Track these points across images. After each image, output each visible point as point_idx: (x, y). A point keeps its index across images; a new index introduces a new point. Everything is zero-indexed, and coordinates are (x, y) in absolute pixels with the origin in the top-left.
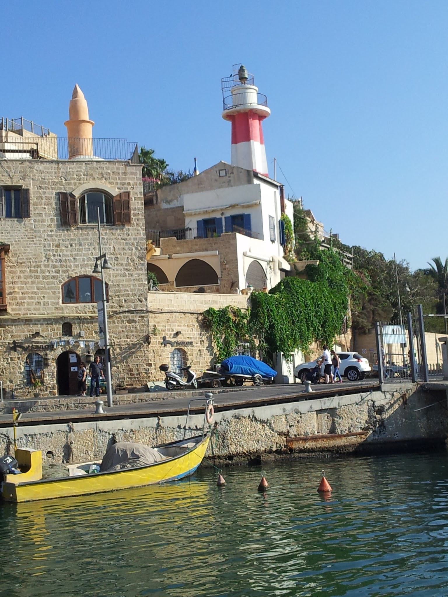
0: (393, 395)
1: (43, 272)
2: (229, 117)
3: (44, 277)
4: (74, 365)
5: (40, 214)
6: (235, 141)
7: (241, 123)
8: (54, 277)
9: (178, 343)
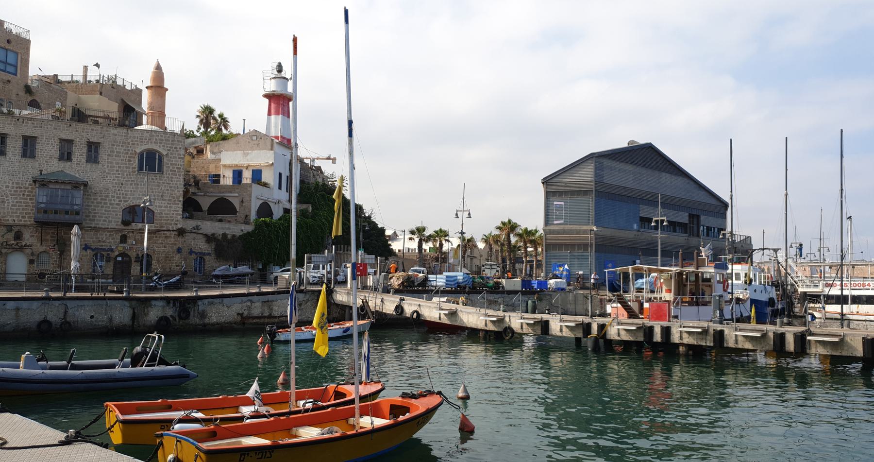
2: (266, 96)
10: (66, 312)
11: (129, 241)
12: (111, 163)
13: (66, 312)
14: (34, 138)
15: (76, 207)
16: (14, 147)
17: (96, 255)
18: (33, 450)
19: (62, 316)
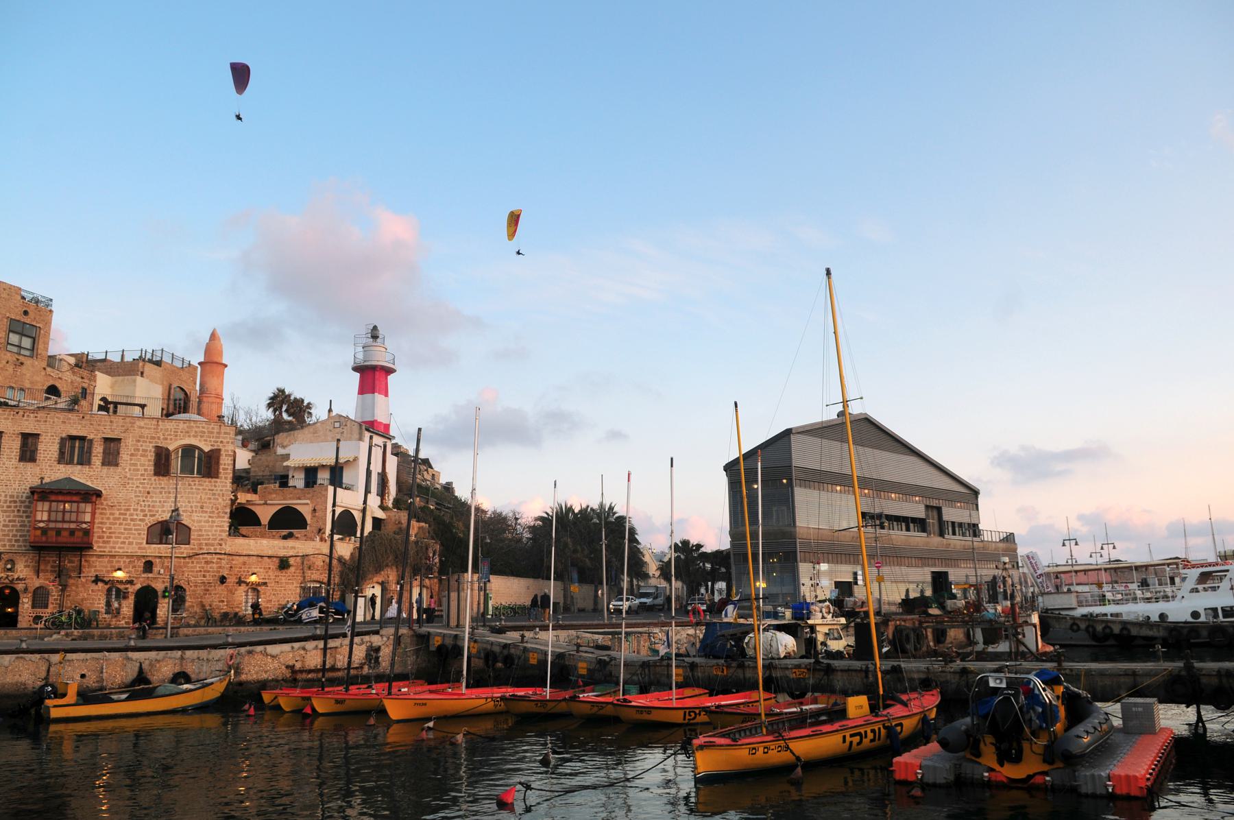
2: (356, 369)
6: (362, 391)
7: (372, 377)
10: (48, 671)
11: (155, 569)
12: (135, 465)
13: (48, 671)
14: (36, 436)
15: (84, 526)
16: (13, 446)
17: (109, 590)
18: (846, 380)
19: (43, 675)
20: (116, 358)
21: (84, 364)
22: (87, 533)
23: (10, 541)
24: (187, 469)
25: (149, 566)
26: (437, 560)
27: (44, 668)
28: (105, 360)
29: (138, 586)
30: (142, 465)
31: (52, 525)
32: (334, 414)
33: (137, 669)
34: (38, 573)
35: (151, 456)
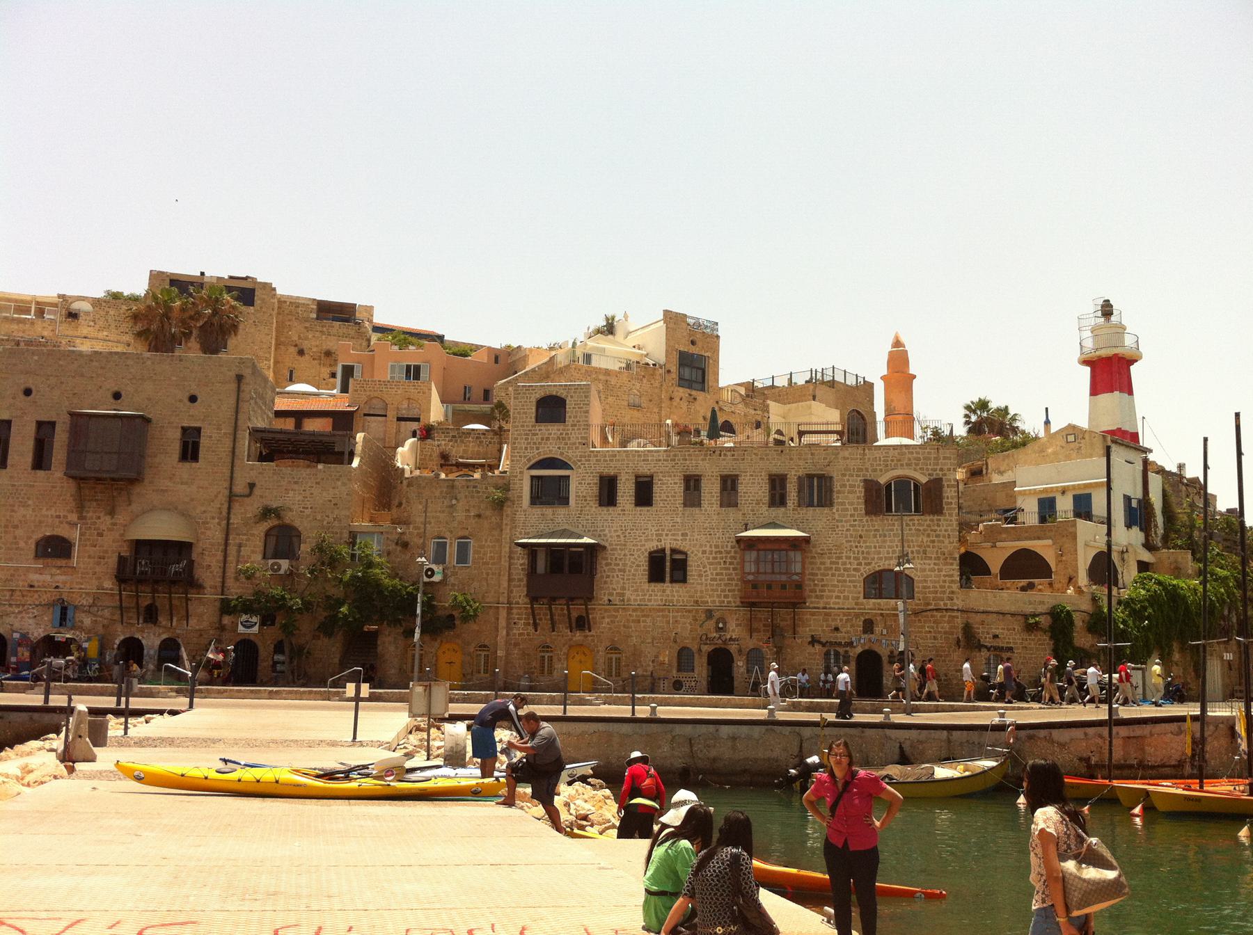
0: (1217, 727)
1: (845, 564)
2: (1086, 362)
3: (845, 570)
4: (358, 690)
5: (843, 504)
6: (1095, 391)
7: (1111, 372)
8: (855, 570)
9: (996, 648)
11: (877, 629)
15: (795, 577)
17: (827, 654)
20: (782, 382)
21: (752, 393)
22: (799, 586)
23: (719, 596)
24: (904, 507)
25: (869, 626)
26: (1234, 620)
27: (796, 743)
28: (773, 387)
29: (859, 650)
30: (852, 504)
31: (762, 578)
32: (1054, 428)
33: (897, 750)
34: (751, 631)
35: (860, 491)
